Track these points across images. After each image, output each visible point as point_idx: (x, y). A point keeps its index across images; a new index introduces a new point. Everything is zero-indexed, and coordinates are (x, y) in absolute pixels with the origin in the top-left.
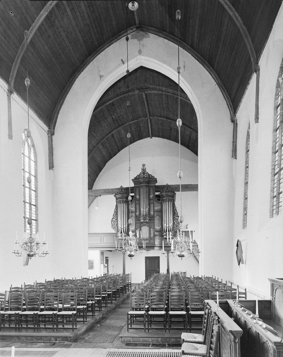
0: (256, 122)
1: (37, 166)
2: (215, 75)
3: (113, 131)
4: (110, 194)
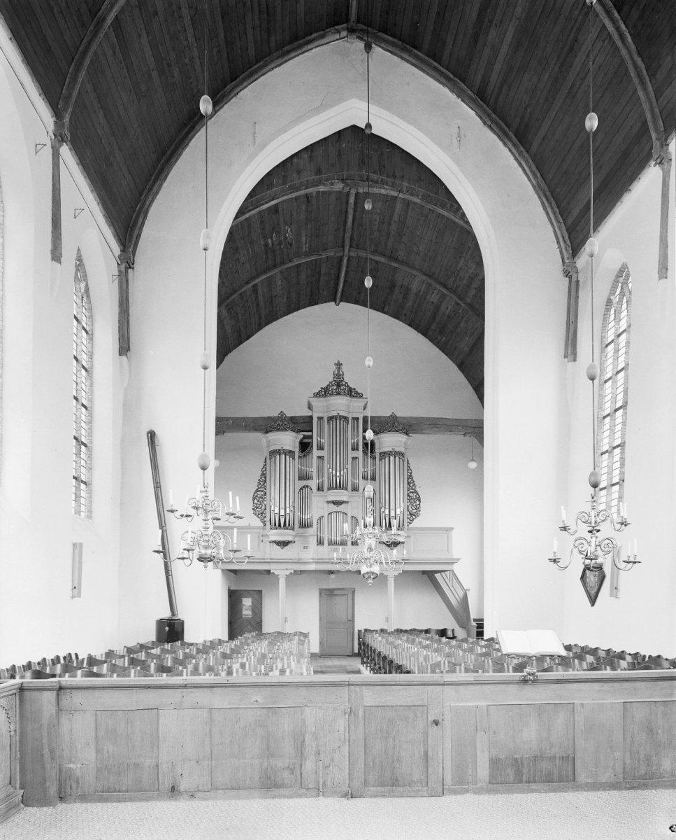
0: (660, 278)
1: (92, 344)
2: (530, 167)
3: (258, 276)
4: (249, 431)
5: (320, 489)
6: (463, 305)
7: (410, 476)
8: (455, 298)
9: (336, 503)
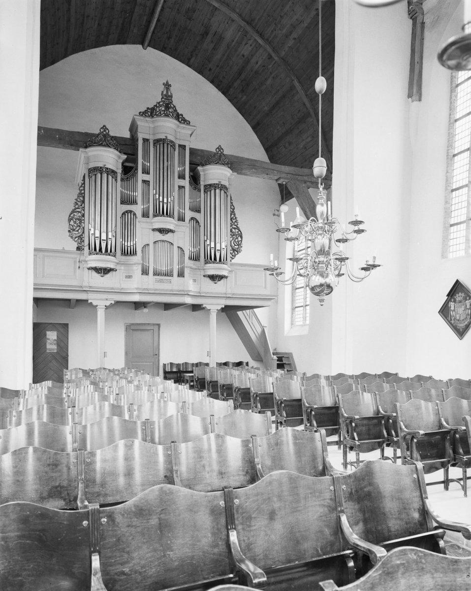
5: (145, 215)
6: (276, 58)
7: (233, 212)
8: (269, 50)
9: (162, 231)
